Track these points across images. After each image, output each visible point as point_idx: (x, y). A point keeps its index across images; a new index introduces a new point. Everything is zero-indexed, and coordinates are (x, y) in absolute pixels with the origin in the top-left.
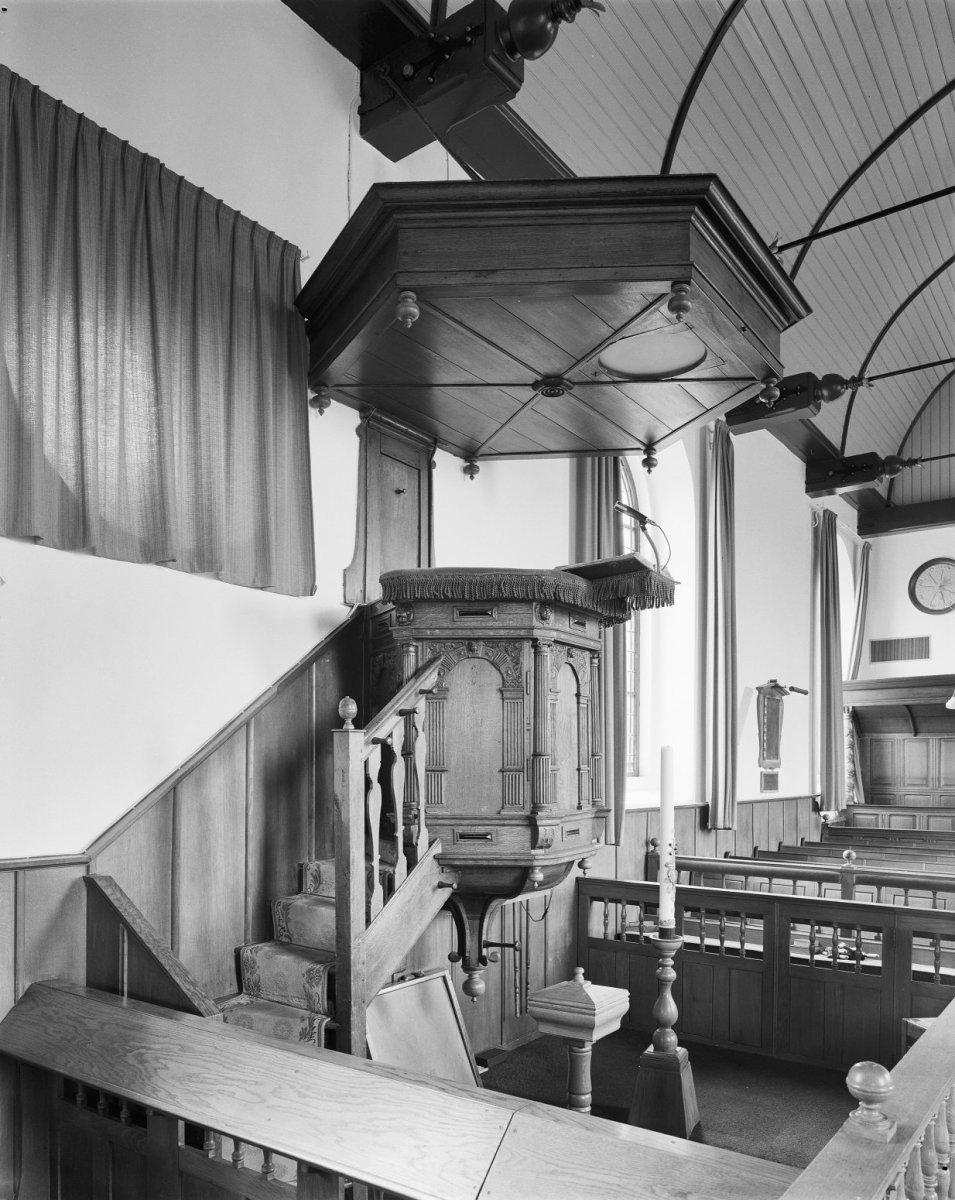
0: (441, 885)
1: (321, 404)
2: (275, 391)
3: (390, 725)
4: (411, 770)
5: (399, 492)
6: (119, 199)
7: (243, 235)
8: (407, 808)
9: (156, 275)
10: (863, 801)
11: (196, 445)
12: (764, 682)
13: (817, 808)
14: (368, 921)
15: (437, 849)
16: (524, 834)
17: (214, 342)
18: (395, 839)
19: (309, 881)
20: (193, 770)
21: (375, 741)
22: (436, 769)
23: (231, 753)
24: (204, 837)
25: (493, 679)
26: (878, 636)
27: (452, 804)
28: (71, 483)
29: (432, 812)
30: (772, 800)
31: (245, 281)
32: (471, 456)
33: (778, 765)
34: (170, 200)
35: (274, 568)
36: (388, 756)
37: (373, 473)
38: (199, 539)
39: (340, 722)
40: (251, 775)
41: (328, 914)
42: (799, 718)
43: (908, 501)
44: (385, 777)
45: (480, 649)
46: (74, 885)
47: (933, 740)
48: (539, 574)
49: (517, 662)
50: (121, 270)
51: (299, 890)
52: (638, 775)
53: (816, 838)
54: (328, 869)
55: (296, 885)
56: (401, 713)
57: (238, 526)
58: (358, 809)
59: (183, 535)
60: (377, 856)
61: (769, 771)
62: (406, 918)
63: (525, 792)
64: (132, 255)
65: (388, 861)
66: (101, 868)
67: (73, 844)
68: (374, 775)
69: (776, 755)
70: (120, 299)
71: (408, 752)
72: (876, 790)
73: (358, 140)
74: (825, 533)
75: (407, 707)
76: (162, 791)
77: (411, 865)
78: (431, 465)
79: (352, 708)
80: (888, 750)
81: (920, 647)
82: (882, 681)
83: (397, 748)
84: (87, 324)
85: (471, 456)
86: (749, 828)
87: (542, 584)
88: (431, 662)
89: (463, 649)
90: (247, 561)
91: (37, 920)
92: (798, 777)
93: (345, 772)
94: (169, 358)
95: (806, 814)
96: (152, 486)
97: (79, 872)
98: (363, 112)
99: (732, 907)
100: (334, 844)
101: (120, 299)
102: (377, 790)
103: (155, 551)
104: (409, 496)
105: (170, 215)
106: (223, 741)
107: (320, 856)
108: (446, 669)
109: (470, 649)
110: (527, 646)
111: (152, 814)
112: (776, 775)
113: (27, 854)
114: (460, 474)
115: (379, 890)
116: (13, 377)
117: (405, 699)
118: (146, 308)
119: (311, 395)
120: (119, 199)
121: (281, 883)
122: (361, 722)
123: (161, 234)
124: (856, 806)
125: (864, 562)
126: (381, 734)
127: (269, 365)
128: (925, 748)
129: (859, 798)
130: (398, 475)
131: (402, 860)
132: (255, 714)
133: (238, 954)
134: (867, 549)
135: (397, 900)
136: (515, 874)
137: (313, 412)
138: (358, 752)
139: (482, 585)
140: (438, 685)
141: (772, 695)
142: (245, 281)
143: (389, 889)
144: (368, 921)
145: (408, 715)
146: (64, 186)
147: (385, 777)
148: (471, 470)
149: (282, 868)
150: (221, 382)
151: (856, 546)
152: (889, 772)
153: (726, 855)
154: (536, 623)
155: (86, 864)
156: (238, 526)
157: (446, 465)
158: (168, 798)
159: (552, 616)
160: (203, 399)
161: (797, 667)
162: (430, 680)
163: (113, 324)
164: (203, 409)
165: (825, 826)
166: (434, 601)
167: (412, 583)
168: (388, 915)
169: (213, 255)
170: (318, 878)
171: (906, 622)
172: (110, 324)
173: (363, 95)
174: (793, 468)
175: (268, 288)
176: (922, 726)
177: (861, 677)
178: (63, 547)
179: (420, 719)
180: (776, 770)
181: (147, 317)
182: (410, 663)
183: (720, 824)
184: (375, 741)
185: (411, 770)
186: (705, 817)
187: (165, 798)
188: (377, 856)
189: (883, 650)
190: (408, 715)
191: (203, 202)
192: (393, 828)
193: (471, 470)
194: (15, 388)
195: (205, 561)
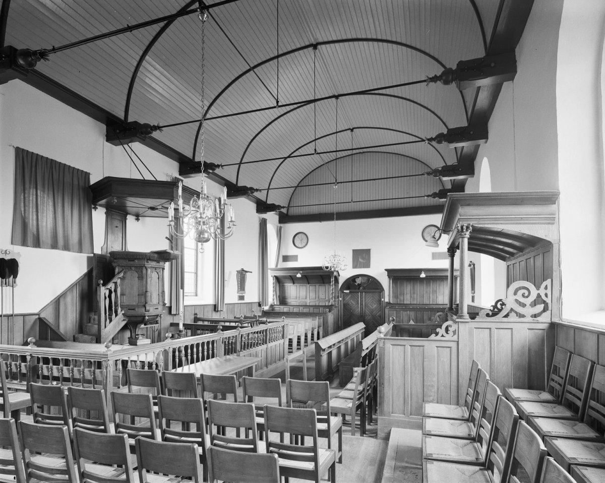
0: (124, 320)
1: (95, 208)
2: (83, 208)
3: (111, 285)
4: (116, 294)
5: (116, 227)
6: (46, 170)
7: (75, 172)
8: (115, 303)
9: (54, 185)
10: (278, 303)
11: (64, 222)
12: (239, 269)
13: (260, 305)
14: (105, 327)
15: (123, 312)
16: (144, 309)
17: (68, 198)
18: (112, 310)
19: (92, 321)
20: (63, 295)
21: (107, 289)
22: (122, 294)
23: (72, 291)
24: (66, 309)
25: (136, 275)
26: (284, 254)
27: (126, 301)
28: (35, 233)
29: (121, 304)
30: (242, 303)
31: (76, 183)
32: (138, 216)
33: (245, 293)
34: (57, 168)
35: (83, 248)
36: (110, 292)
37: (109, 223)
38: (65, 243)
39: (99, 285)
40: (77, 296)
41: (96, 326)
42: (252, 281)
43: (292, 214)
44: (110, 296)
45: (133, 268)
46: (36, 319)
47: (298, 285)
48: (146, 253)
49: (142, 272)
50: (46, 186)
51: (89, 323)
52: (197, 296)
53: (261, 315)
54: (96, 317)
55: (89, 321)
56: (114, 283)
57: (74, 238)
58: (103, 304)
59: (61, 242)
60: (108, 313)
61: (241, 295)
62: (115, 327)
63: (143, 300)
64: (49, 181)
65: (110, 315)
66: (42, 316)
67: (36, 311)
68: (107, 296)
69: (244, 290)
70: (46, 186)
71: (116, 291)
72: (283, 300)
73: (105, 142)
74: (263, 224)
75: (115, 281)
76: (56, 300)
77: (116, 315)
78: (126, 219)
79: (102, 282)
80: (286, 289)
81: (295, 258)
82: (286, 268)
83: (113, 290)
84: (39, 192)
85: (138, 216)
86: (232, 311)
87: (146, 256)
88: (122, 271)
89: (129, 268)
90: (77, 247)
91: (28, 327)
92: (252, 295)
93: (100, 295)
94: (58, 203)
95: (256, 308)
96: (53, 232)
97: (37, 317)
98: (107, 136)
99: (206, 328)
100: (97, 311)
101: (46, 186)
102: (108, 300)
103: (54, 246)
104: (120, 227)
105: (57, 171)
106: (71, 288)
107: (95, 315)
108: (125, 273)
109: (131, 268)
110: (144, 268)
111: (548, 324)
112: (244, 296)
113: (27, 312)
114: (135, 221)
115: (108, 321)
116: (23, 212)
117: (115, 280)
118: (52, 193)
119: (93, 206)
120: (46, 170)
121: (85, 321)
122: (104, 285)
123: (56, 176)
124: (275, 305)
125: (279, 233)
126: (109, 287)
127: (82, 200)
128: (314, 289)
129: (276, 302)
130: (117, 223)
131: (114, 314)
132: (78, 282)
133: (74, 336)
134: (281, 228)
135: (112, 323)
136: (142, 318)
137: (93, 210)
138: (103, 291)
139: (133, 255)
140: (123, 277)
141: (242, 275)
142: (76, 183)
143: (111, 321)
144: (105, 327)
145: (116, 283)
146: (33, 169)
147: (110, 296)
148: (138, 219)
149: (85, 317)
150: (70, 207)
151: (278, 227)
152: (287, 295)
153: (235, 318)
154: (146, 263)
155: (38, 314)
156: (74, 238)
157: (130, 219)
158: (57, 302)
159: (150, 262)
160: (66, 212)
161: (252, 264)
162: (121, 275)
163: (45, 188)
164: (65, 214)
165: (263, 311)
166: (122, 258)
167: (117, 255)
168: (110, 326)
169: (68, 178)
170: (94, 320)
171: (291, 251)
172: (44, 192)
173: (107, 132)
174: (253, 206)
175: (82, 184)
176: (295, 282)
177: (279, 267)
178: (34, 247)
179: (118, 284)
180: (244, 295)
181: (52, 195)
182: (117, 270)
183: (219, 310)
184: (107, 289)
185: (116, 294)
186: (215, 308)
187: (57, 301)
188: (108, 313)
189: (286, 259)
190: (116, 283)
191: (66, 167)
192: (112, 307)
193: (138, 219)
194: (23, 215)
195: (66, 248)
